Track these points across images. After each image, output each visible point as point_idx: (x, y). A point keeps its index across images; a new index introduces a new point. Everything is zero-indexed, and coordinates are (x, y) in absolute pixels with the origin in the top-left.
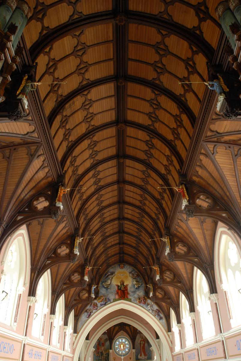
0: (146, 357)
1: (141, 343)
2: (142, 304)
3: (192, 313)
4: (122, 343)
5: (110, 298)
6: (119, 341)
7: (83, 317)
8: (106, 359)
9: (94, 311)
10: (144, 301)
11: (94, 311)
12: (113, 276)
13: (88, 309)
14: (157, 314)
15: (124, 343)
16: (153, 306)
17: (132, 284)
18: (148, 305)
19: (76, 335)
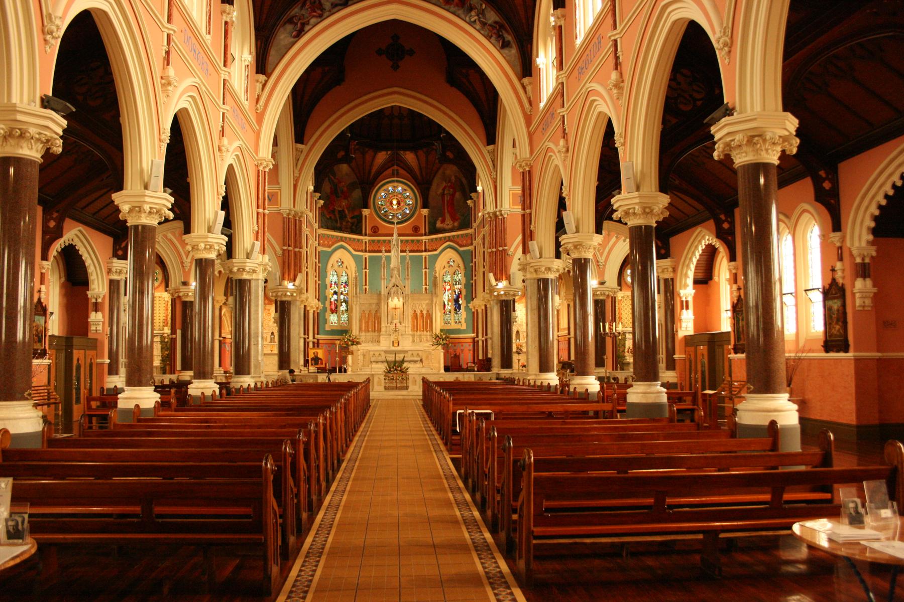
0: (456, 224)
4: (395, 194)
7: (283, 36)
9: (313, 21)
11: (313, 21)
15: (401, 194)
18: (471, 9)
19: (262, 78)
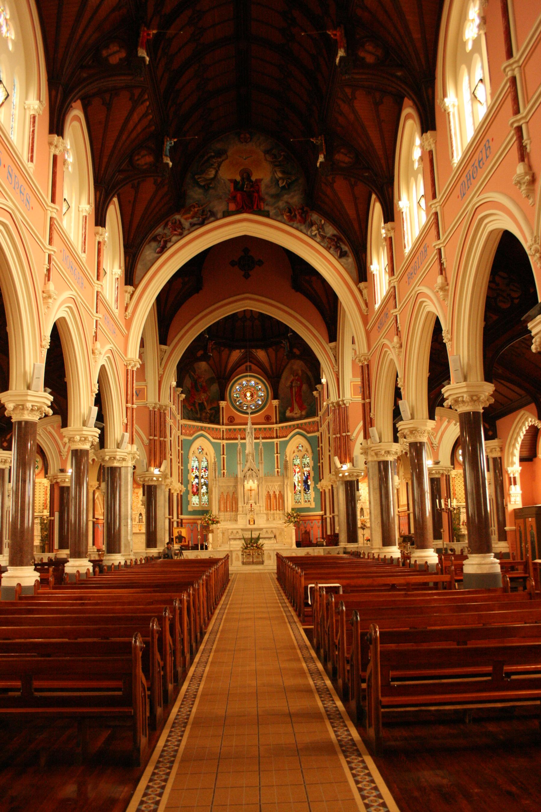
0: (304, 413)
1: (293, 385)
2: (295, 222)
3: (429, 133)
4: (248, 387)
5: (215, 210)
6: (241, 384)
7: (148, 252)
8: (212, 418)
9: (174, 238)
10: (301, 216)
11: (174, 238)
12: (223, 161)
13: (159, 235)
14: (333, 245)
16: (325, 227)
17: (272, 179)
18: (312, 224)
19: (130, 289)
